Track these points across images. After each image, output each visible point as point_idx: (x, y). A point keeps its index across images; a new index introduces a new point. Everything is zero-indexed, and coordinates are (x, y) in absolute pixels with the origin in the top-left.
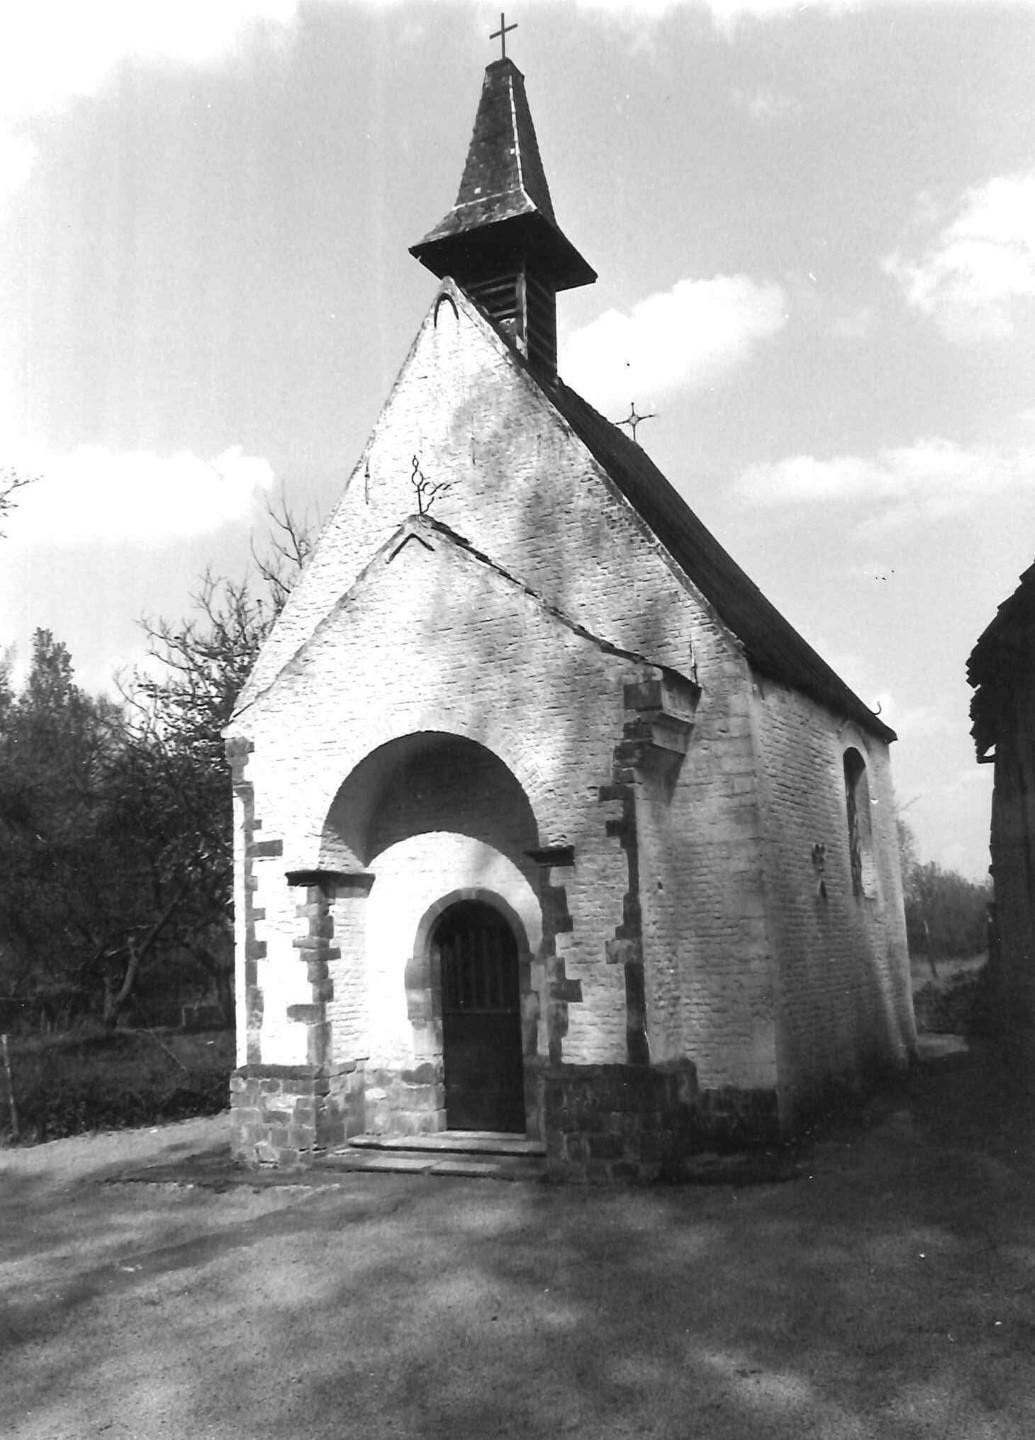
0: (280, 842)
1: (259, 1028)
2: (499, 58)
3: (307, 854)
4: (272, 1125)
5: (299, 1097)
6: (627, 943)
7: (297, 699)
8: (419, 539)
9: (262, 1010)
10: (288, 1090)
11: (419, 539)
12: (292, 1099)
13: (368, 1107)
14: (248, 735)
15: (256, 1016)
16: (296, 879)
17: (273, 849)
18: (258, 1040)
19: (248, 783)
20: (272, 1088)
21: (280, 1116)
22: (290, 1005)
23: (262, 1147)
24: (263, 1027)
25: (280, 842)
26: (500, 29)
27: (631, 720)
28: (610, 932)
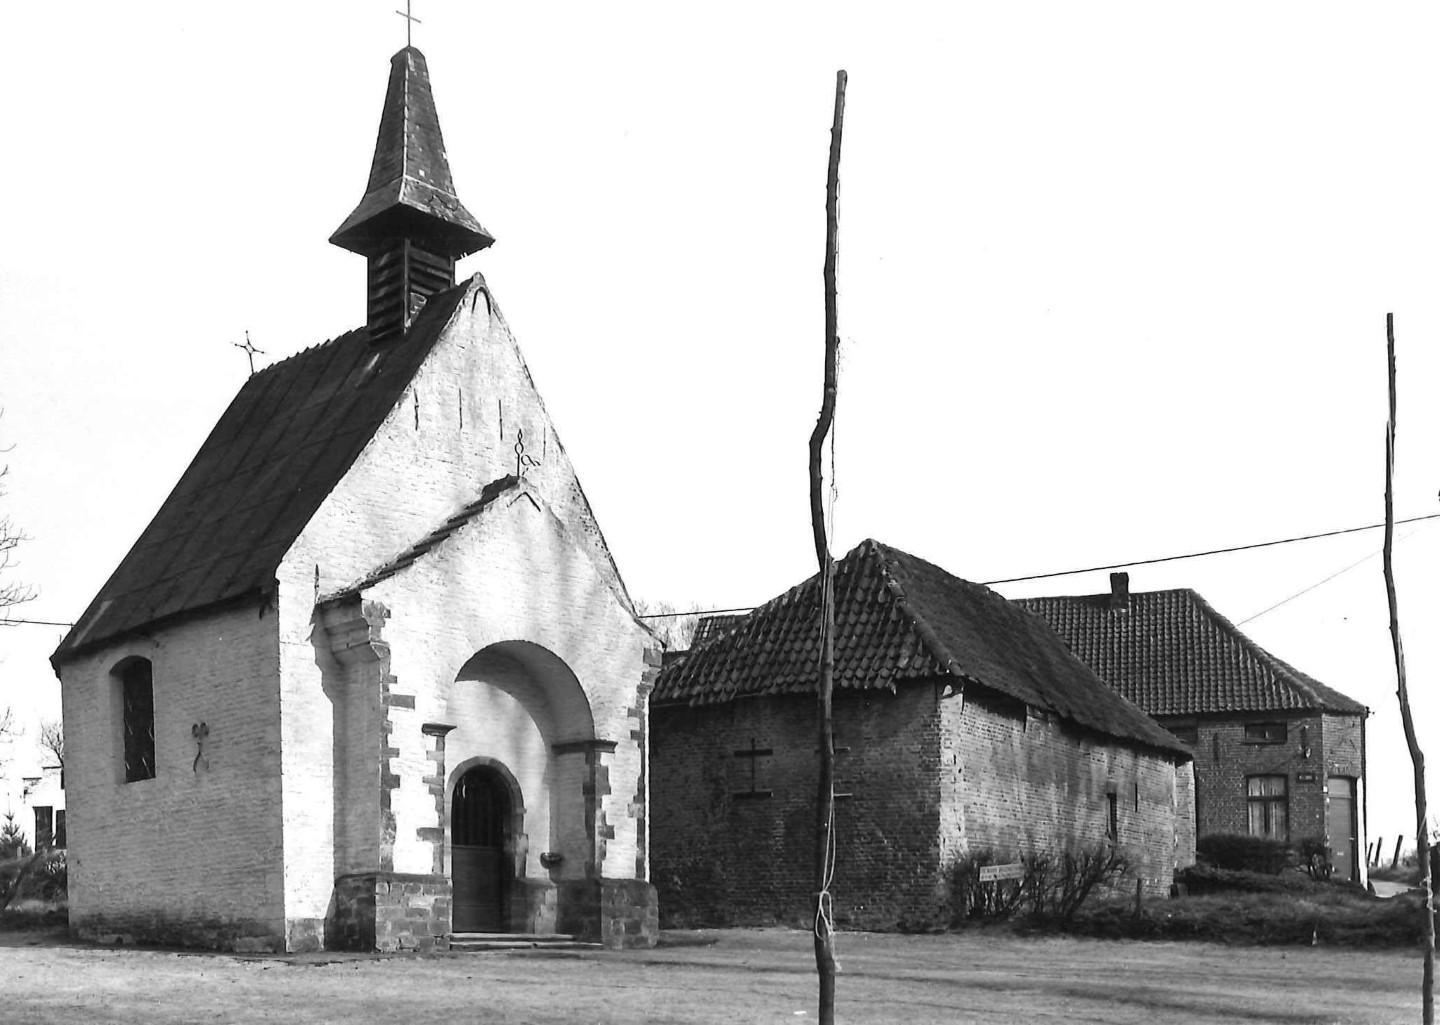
0: (413, 698)
1: (393, 843)
2: (405, 45)
3: (430, 709)
4: (413, 919)
5: (436, 897)
6: (639, 805)
7: (430, 585)
8: (1287, 815)
9: (395, 829)
10: (427, 892)
11: (1287, 815)
12: (431, 899)
13: (1136, 757)
14: (386, 603)
15: (390, 834)
16: (428, 729)
17: (407, 702)
18: (392, 853)
19: (384, 643)
20: (414, 891)
21: (421, 912)
22: (419, 827)
23: (404, 936)
24: (396, 843)
25: (413, 698)
26: (412, 15)
27: (647, 670)
28: (630, 798)
